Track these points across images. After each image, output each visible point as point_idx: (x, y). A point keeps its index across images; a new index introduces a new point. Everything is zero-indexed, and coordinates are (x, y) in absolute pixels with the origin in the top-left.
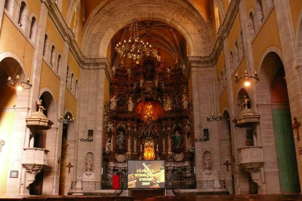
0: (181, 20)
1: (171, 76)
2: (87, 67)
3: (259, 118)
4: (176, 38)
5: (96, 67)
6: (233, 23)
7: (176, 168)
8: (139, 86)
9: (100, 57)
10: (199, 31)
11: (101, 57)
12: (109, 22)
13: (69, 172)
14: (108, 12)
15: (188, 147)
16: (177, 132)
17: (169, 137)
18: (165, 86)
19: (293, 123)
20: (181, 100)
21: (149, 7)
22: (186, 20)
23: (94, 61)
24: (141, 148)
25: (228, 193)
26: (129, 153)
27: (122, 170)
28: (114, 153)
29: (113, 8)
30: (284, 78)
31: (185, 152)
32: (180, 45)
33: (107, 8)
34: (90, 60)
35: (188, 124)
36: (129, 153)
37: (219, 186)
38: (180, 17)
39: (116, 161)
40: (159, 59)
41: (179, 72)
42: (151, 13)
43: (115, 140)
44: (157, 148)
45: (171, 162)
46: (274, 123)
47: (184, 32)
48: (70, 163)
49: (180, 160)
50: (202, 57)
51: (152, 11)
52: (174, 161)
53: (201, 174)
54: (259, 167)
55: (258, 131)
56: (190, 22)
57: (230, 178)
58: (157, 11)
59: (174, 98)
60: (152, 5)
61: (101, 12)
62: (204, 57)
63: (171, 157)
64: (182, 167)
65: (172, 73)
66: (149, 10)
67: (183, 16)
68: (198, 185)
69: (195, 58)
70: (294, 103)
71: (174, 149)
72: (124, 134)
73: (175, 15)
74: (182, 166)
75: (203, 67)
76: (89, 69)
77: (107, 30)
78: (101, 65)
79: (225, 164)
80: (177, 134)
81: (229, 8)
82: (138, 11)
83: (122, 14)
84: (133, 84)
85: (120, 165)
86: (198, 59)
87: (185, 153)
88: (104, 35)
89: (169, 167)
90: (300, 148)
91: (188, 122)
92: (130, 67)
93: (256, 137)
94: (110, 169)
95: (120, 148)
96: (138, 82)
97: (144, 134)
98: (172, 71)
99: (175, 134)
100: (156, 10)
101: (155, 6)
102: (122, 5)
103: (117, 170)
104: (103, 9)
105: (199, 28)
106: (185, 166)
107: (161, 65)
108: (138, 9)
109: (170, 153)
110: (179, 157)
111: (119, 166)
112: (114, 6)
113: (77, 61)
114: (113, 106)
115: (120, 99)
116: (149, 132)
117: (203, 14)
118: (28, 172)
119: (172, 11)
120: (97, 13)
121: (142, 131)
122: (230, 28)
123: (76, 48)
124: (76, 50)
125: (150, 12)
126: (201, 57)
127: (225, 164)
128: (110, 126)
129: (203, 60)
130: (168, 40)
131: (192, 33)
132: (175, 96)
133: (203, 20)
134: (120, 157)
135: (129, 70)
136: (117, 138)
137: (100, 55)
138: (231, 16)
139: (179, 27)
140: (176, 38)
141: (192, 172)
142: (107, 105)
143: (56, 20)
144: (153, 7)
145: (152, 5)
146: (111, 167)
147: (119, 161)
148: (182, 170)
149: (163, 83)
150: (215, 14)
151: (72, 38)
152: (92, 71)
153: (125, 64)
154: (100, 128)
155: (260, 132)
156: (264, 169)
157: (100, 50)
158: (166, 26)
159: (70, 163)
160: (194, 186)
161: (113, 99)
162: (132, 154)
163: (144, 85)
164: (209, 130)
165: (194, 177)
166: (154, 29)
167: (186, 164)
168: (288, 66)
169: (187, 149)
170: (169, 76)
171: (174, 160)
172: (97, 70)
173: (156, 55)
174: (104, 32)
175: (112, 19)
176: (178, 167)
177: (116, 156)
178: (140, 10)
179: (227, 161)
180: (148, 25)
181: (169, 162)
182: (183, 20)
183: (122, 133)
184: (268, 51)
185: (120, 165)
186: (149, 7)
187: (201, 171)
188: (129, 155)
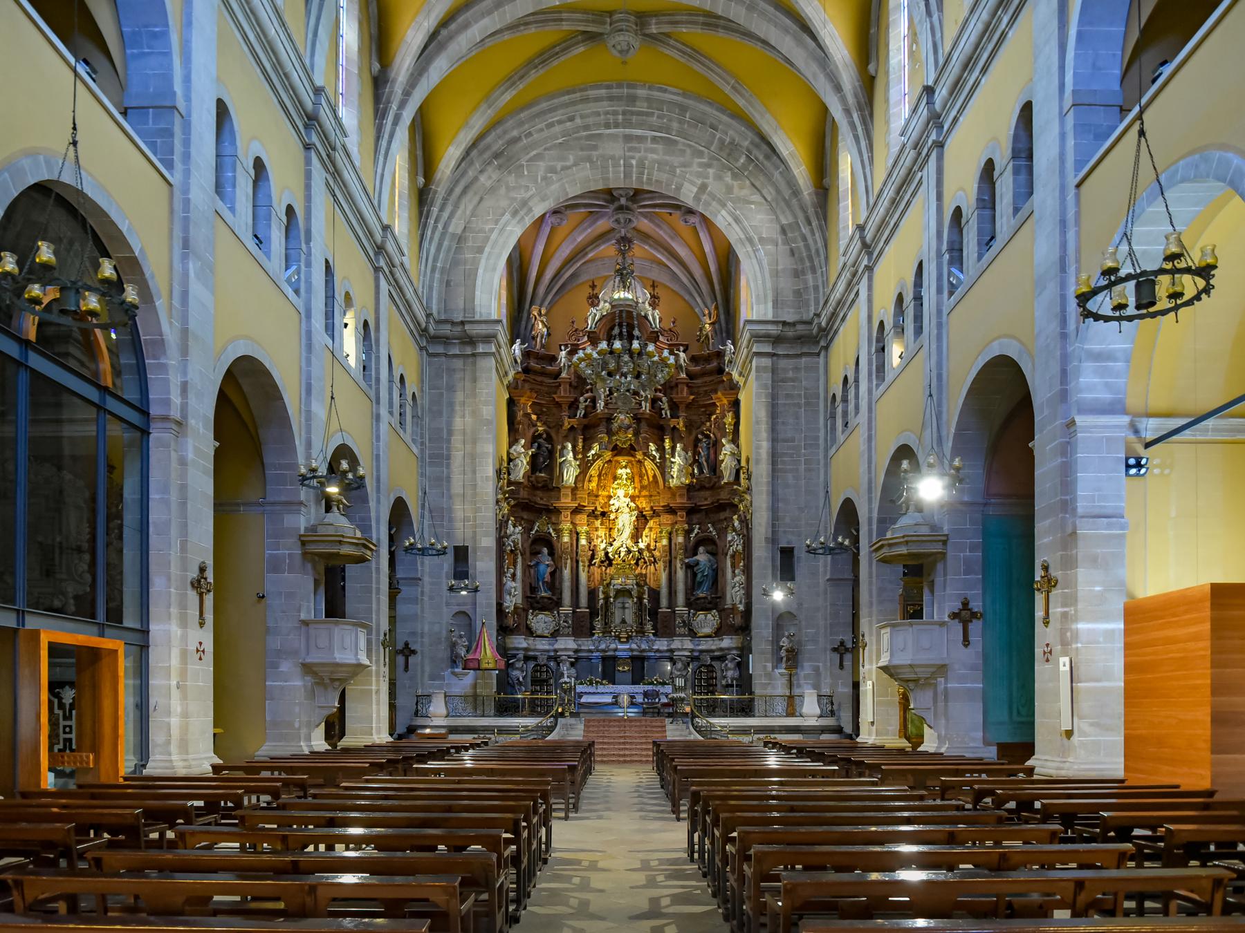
0: (729, 189)
1: (691, 376)
2: (440, 349)
3: (945, 543)
4: (707, 247)
5: (469, 351)
6: (896, 225)
7: (696, 654)
8: (594, 407)
9: (477, 318)
10: (783, 231)
11: (484, 318)
12: (503, 191)
13: (406, 668)
14: (497, 156)
15: (734, 594)
16: (701, 549)
17: (679, 565)
18: (671, 409)
19: (1037, 578)
20: (716, 454)
21: (628, 138)
22: (746, 192)
23: (459, 329)
24: (601, 596)
25: (838, 730)
26: (566, 609)
27: (550, 658)
28: (525, 610)
29: (516, 140)
30: (1030, 445)
31: (724, 609)
32: (720, 269)
33: (495, 142)
34: (449, 327)
35: (734, 530)
36: (566, 609)
37: (818, 711)
38: (728, 178)
39: (530, 632)
40: (654, 319)
41: (715, 364)
42: (634, 162)
43: (527, 568)
44: (646, 596)
45: (684, 635)
46: (985, 558)
47: (734, 235)
48: (407, 644)
49: (707, 630)
50: (789, 324)
51: (637, 155)
52: (693, 634)
53: (769, 676)
54: (933, 676)
55: (939, 580)
56: (756, 197)
57: (848, 690)
58: (655, 156)
59: (696, 446)
60: (639, 132)
61: (474, 153)
62: (794, 324)
63: (684, 622)
64: (713, 651)
65: (693, 368)
66: (630, 149)
67: (735, 176)
68: (759, 705)
69: (770, 327)
70: (1047, 522)
71: (693, 598)
72: (551, 554)
73: (711, 171)
74: (713, 647)
75: (787, 356)
76: (446, 355)
77: (497, 222)
78: (484, 342)
79: (835, 650)
80: (702, 557)
81: (890, 175)
82: (594, 153)
83: (541, 163)
84: (577, 400)
85: (542, 645)
86: (773, 330)
87: (721, 611)
88: (488, 238)
89: (679, 650)
90: (1047, 645)
91: (736, 523)
92: (566, 346)
93: (932, 592)
94: (514, 656)
95: (543, 594)
96: (589, 394)
97: (607, 554)
98: (694, 359)
99: (695, 554)
100: (653, 151)
101: (646, 138)
102: (542, 130)
103: (535, 658)
104: (482, 145)
105: (784, 222)
106: (721, 649)
107: (661, 338)
108: (595, 148)
109: (681, 608)
110: (707, 622)
111: (540, 647)
112: (515, 133)
113: (411, 332)
114: (522, 468)
115: (539, 447)
116: (623, 550)
117: (801, 172)
118: (317, 683)
119: (700, 154)
120: (463, 159)
121: (603, 546)
122: (887, 242)
123: (405, 289)
124: (408, 296)
125: (633, 158)
126: (784, 323)
127: (835, 650)
128: (515, 532)
129: (790, 333)
130: (682, 252)
131: (761, 240)
132: (700, 440)
133: (796, 192)
134: (541, 622)
135: (563, 353)
136: (530, 566)
137: (478, 309)
138: (894, 202)
139: (722, 220)
140: (707, 247)
141: (742, 666)
142: (504, 469)
143: (286, 91)
144: (640, 139)
145: (639, 132)
146: (518, 649)
147: (539, 632)
148: (713, 659)
149: (664, 399)
150: (841, 175)
151: (397, 261)
152: (458, 363)
153: (549, 334)
154: (488, 542)
155: (945, 581)
156: (946, 683)
157: (478, 293)
158: (678, 207)
159: (407, 644)
160: (746, 709)
161: (519, 448)
162: (574, 612)
163: (610, 406)
164: (796, 552)
165: (744, 683)
166: (645, 215)
167: (727, 642)
168: (1046, 412)
169: (729, 601)
170: (683, 375)
171: (690, 630)
172: (471, 360)
173: (647, 305)
174: (487, 227)
175: (511, 179)
176: (701, 651)
177: (530, 617)
178: (600, 152)
179: (842, 643)
180: (623, 201)
181: (680, 635)
182: (736, 190)
183: (545, 550)
184: (995, 351)
186: (628, 138)
187: (769, 665)
188: (566, 615)
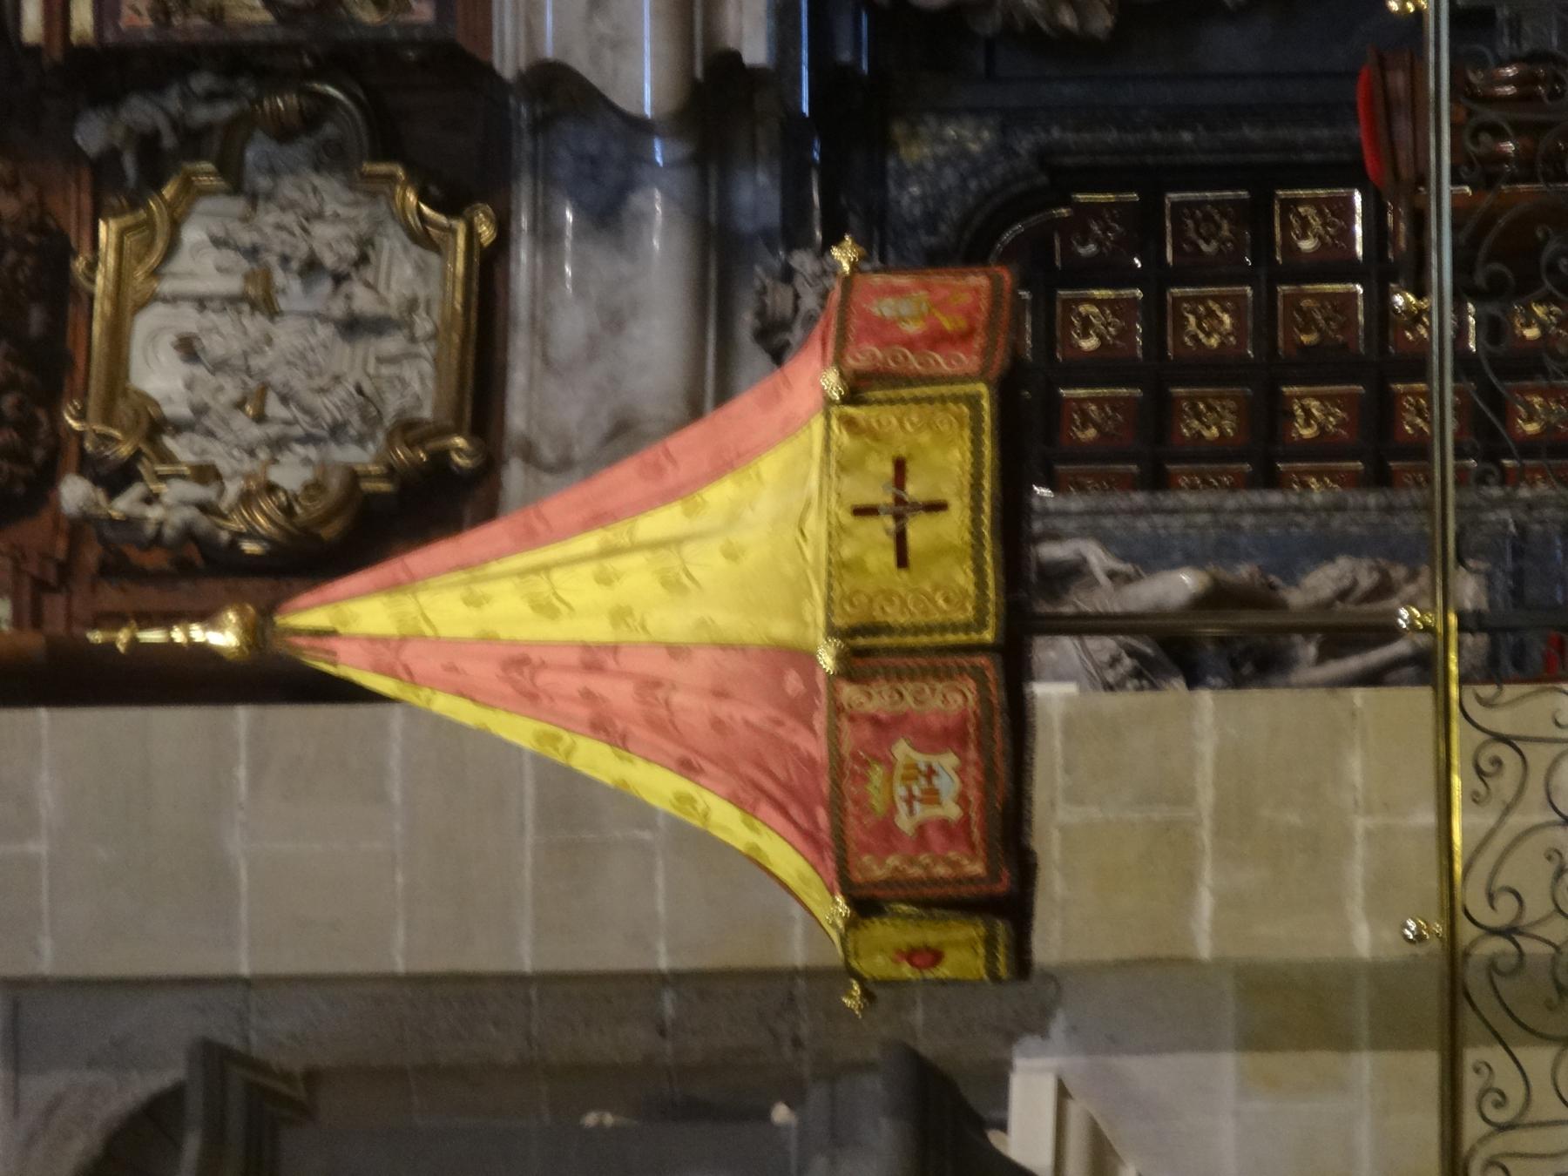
147: (417, 382)
177: (168, 505)
185: (615, 321)
